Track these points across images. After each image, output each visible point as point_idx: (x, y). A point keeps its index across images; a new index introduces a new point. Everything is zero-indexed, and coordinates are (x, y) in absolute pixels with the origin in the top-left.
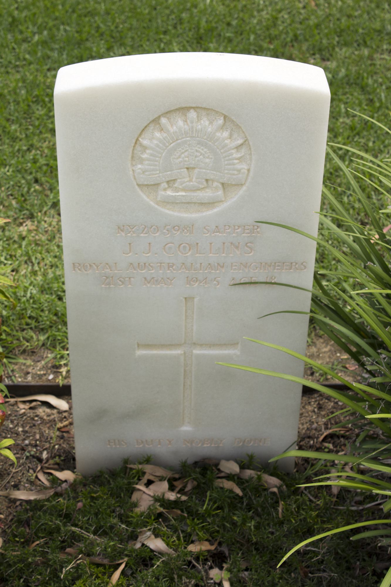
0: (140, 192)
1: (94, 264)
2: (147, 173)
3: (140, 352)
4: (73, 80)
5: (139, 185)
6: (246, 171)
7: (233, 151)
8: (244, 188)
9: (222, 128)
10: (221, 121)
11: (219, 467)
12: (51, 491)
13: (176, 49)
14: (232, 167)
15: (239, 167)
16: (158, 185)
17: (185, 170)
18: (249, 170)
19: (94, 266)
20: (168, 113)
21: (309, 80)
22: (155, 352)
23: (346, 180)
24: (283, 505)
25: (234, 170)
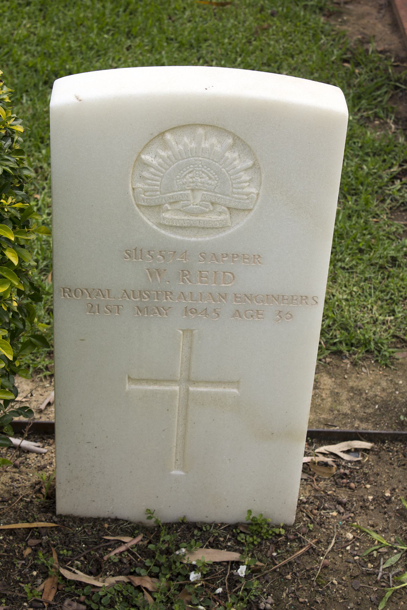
0: (141, 214)
1: (87, 289)
2: (147, 194)
3: (130, 387)
4: (70, 92)
5: (138, 206)
6: (255, 196)
7: (242, 173)
8: (252, 213)
9: (231, 148)
10: (230, 141)
11: (64, 505)
12: (398, 555)
13: (165, 60)
14: (240, 190)
15: (247, 190)
16: (160, 206)
17: (189, 192)
18: (258, 194)
19: (85, 291)
20: (172, 130)
21: (329, 100)
22: (220, 390)
23: (51, 199)
24: (190, 550)
25: (243, 194)
